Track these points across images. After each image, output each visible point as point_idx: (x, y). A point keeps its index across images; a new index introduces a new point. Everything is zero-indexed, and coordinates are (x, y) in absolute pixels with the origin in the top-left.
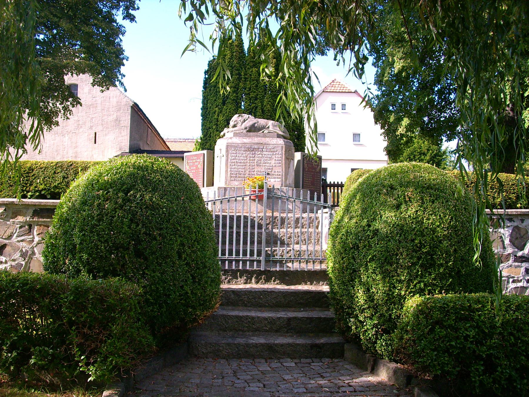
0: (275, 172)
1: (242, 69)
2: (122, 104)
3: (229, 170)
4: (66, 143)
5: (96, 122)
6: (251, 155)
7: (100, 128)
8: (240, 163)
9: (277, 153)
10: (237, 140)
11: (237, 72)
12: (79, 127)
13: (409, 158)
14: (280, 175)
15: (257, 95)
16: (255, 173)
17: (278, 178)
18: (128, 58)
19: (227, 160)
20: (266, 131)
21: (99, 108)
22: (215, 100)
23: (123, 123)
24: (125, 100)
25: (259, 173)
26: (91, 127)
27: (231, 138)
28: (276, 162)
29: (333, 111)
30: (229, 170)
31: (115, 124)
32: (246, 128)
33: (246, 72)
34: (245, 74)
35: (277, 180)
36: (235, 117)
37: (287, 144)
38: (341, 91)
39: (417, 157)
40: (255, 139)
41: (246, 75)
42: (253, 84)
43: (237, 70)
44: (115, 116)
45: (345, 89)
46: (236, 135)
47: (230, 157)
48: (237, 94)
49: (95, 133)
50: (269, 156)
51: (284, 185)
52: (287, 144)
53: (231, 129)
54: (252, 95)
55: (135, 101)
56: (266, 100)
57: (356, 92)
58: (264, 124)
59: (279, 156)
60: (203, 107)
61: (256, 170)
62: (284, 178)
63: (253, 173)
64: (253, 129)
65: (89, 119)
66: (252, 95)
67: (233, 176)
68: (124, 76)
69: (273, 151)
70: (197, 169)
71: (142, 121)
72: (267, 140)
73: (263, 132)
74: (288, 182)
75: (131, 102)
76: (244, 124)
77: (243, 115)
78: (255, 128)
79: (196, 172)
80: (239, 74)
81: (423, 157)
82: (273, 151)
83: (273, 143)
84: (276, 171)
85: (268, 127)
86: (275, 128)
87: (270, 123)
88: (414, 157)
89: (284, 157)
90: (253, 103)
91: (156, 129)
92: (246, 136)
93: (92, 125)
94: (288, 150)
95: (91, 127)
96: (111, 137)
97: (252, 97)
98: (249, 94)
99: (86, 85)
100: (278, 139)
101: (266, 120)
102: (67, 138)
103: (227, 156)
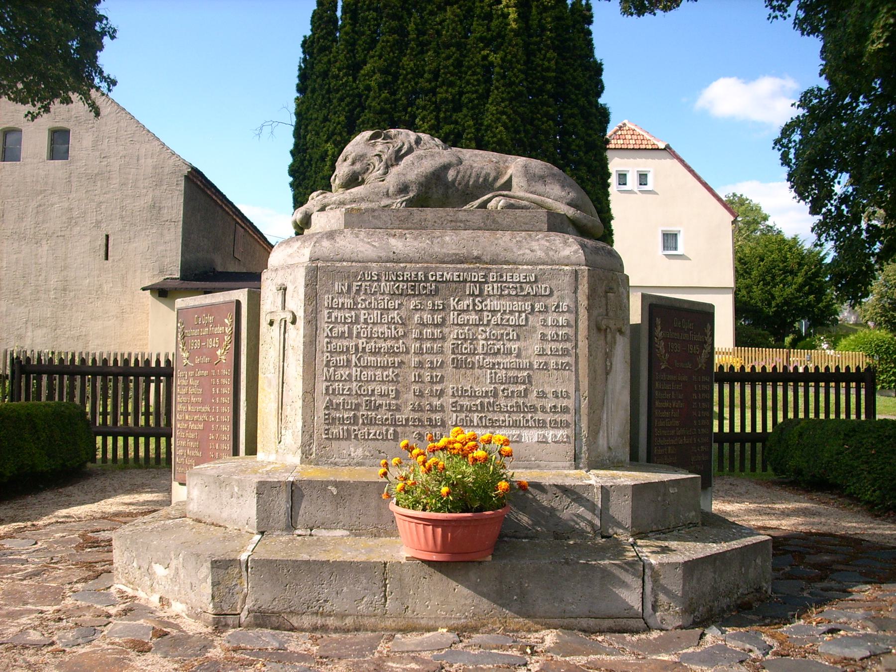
0: (542, 395)
1: (410, 15)
2: (166, 170)
3: (321, 386)
4: (44, 260)
5: (109, 212)
6: (427, 317)
7: (117, 225)
8: (376, 353)
9: (552, 302)
10: (359, 245)
11: (394, 23)
12: (71, 222)
13: (764, 280)
14: (565, 410)
15: (461, 94)
16: (448, 400)
17: (556, 425)
18: (115, 31)
19: (311, 342)
20: (496, 203)
21: (115, 181)
22: (326, 119)
23: (166, 214)
24: (171, 162)
25: (466, 402)
26: (98, 224)
27: (331, 235)
28: (548, 346)
29: (623, 188)
30: (321, 386)
31: (149, 215)
32: (403, 189)
33: (424, 23)
34: (421, 33)
35: (550, 434)
36: (358, 143)
37: (599, 259)
38: (637, 147)
39: (778, 279)
40: (445, 239)
41: (424, 34)
42: (448, 58)
43: (394, 17)
44: (149, 199)
45: (645, 142)
46: (356, 219)
47: (324, 327)
48: (393, 93)
49: (107, 236)
50: (513, 319)
51: (584, 456)
52: (599, 259)
53: (336, 195)
54: (443, 93)
55: (195, 165)
56: (493, 109)
57: (667, 148)
58: (489, 169)
59: (561, 320)
60: (296, 145)
61: (450, 387)
62: (584, 425)
63: (436, 402)
64: (436, 193)
65: (94, 205)
66: (443, 93)
67: (334, 419)
68: (114, 83)
69: (529, 292)
70: (214, 363)
71: (218, 208)
72: (504, 242)
73: (484, 205)
74: (602, 442)
75: (185, 167)
76: (394, 170)
77: (393, 131)
78: (448, 186)
79: (210, 375)
80: (402, 32)
81: (790, 278)
82: (529, 292)
83: (529, 256)
84: (549, 390)
85: (508, 185)
86: (540, 187)
87: (515, 166)
88: (773, 278)
89: (583, 324)
90: (447, 120)
91: (255, 228)
92: (403, 224)
93: (99, 218)
94: (600, 291)
95: (98, 224)
96: (141, 244)
97: (445, 101)
98: (433, 92)
99: (87, 130)
100: (557, 239)
101: (494, 156)
102: (46, 248)
103: (312, 322)
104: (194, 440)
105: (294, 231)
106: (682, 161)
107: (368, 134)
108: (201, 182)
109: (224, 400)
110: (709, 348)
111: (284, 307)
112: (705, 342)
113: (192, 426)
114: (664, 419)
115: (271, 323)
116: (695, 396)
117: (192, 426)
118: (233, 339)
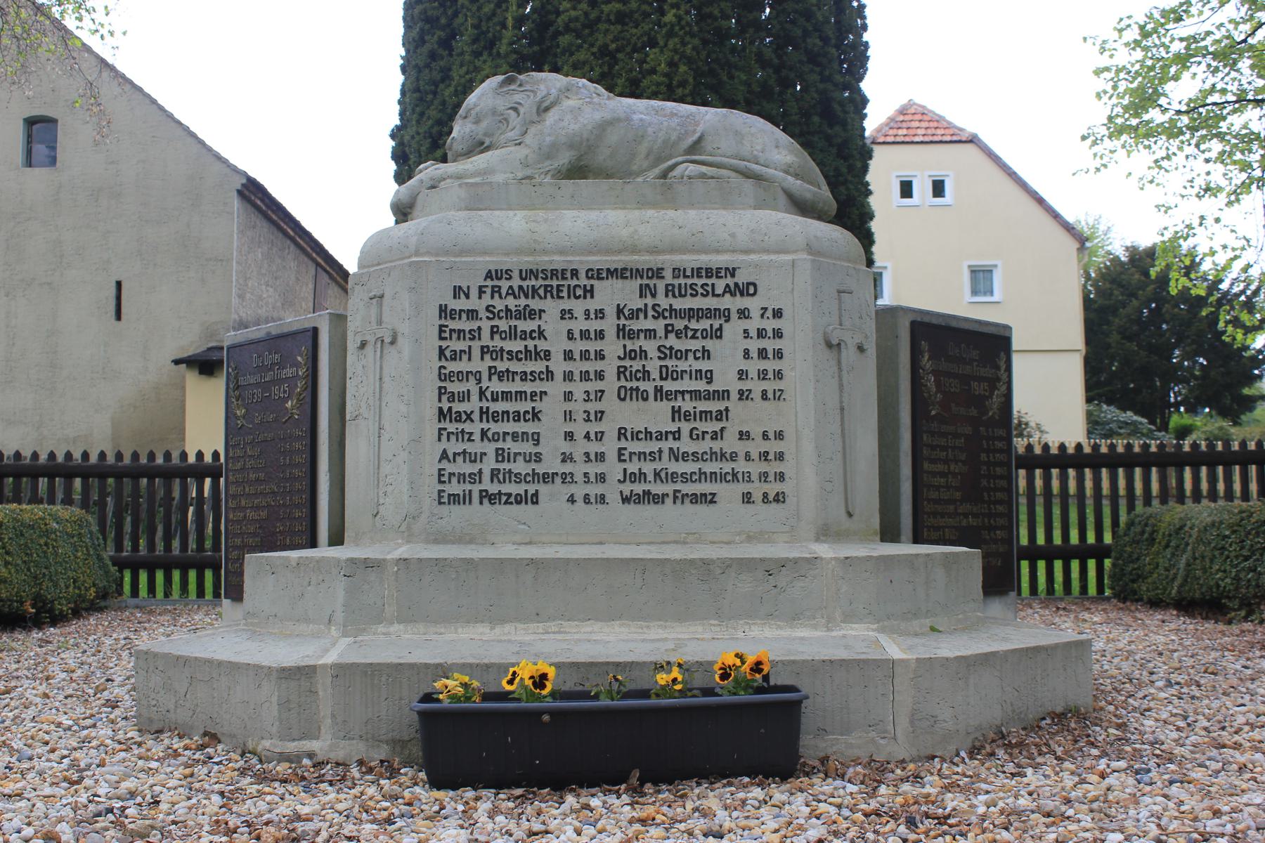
49: (119, 284)
55: (252, 174)
104: (254, 535)
105: (393, 219)
106: (1056, 216)
107: (500, 78)
108: (262, 201)
109: (296, 472)
110: (1003, 388)
111: (380, 322)
112: (999, 380)
113: (251, 514)
114: (938, 488)
115: (363, 345)
116: (983, 457)
117: (251, 514)
118: (310, 383)
